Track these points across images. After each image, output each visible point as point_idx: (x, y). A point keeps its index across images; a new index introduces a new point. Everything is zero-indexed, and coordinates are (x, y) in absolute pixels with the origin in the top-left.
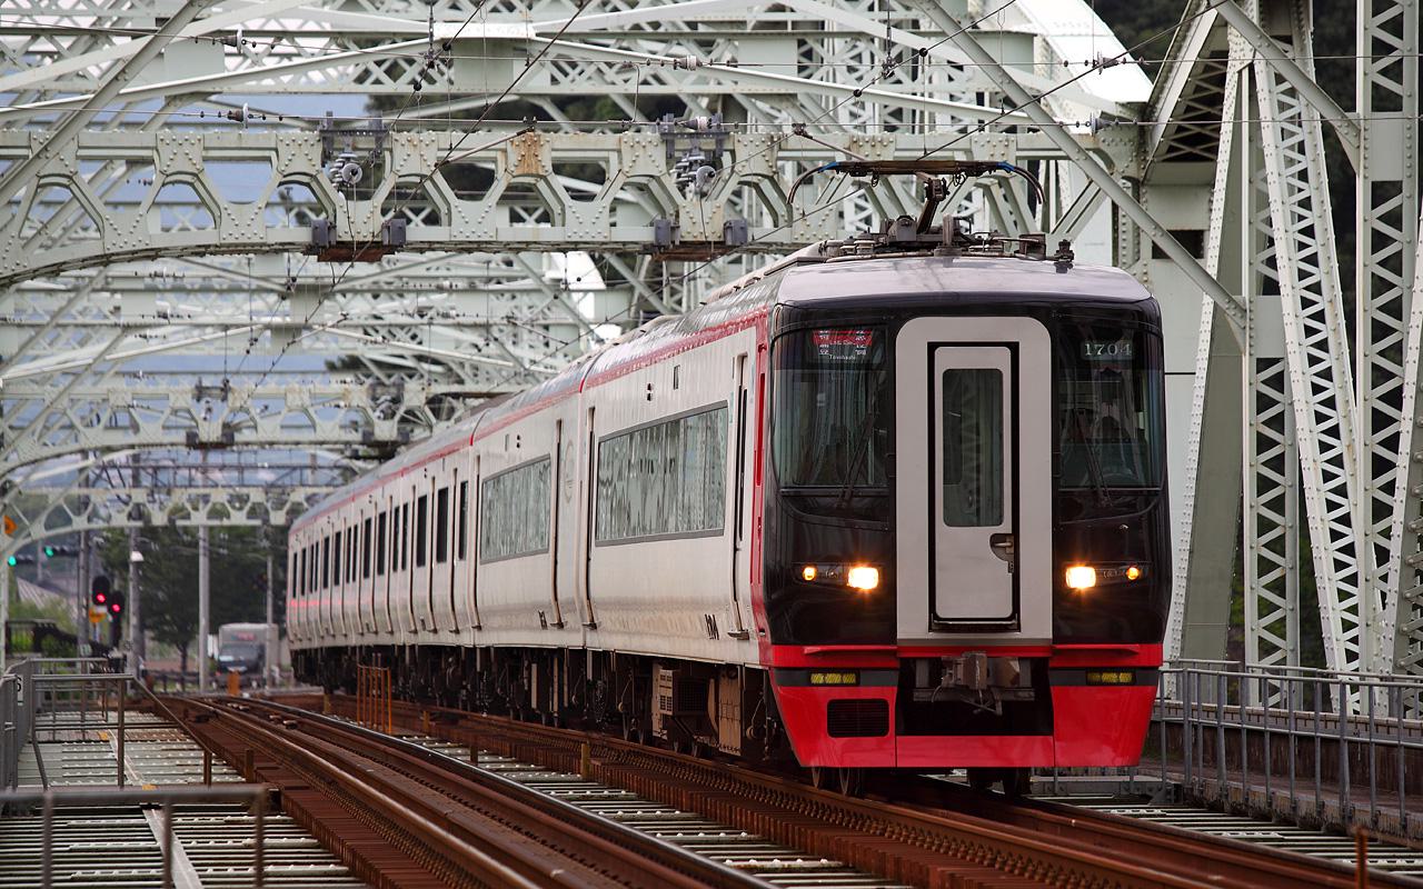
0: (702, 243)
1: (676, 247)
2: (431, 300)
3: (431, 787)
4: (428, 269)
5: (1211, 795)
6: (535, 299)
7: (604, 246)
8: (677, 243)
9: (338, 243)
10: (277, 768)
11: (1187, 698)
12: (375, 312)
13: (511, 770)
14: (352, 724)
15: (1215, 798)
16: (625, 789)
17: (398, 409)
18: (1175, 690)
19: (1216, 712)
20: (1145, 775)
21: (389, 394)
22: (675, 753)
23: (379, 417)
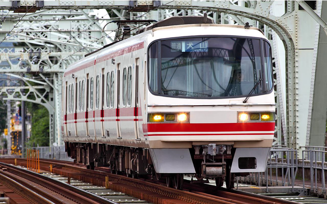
0: (145, 6)
1: (137, 7)
2: (50, 23)
3: (55, 192)
4: (49, 12)
5: (320, 192)
6: (86, 22)
7: (112, 7)
8: (137, 6)
9: (21, 6)
10: (2, 185)
11: (312, 159)
12: (31, 28)
13: (81, 185)
14: (25, 169)
15: (321, 194)
16: (121, 192)
17: (39, 60)
18: (307, 157)
19: (321, 164)
20: (297, 186)
21: (36, 55)
22: (127, 177)
23: (33, 63)
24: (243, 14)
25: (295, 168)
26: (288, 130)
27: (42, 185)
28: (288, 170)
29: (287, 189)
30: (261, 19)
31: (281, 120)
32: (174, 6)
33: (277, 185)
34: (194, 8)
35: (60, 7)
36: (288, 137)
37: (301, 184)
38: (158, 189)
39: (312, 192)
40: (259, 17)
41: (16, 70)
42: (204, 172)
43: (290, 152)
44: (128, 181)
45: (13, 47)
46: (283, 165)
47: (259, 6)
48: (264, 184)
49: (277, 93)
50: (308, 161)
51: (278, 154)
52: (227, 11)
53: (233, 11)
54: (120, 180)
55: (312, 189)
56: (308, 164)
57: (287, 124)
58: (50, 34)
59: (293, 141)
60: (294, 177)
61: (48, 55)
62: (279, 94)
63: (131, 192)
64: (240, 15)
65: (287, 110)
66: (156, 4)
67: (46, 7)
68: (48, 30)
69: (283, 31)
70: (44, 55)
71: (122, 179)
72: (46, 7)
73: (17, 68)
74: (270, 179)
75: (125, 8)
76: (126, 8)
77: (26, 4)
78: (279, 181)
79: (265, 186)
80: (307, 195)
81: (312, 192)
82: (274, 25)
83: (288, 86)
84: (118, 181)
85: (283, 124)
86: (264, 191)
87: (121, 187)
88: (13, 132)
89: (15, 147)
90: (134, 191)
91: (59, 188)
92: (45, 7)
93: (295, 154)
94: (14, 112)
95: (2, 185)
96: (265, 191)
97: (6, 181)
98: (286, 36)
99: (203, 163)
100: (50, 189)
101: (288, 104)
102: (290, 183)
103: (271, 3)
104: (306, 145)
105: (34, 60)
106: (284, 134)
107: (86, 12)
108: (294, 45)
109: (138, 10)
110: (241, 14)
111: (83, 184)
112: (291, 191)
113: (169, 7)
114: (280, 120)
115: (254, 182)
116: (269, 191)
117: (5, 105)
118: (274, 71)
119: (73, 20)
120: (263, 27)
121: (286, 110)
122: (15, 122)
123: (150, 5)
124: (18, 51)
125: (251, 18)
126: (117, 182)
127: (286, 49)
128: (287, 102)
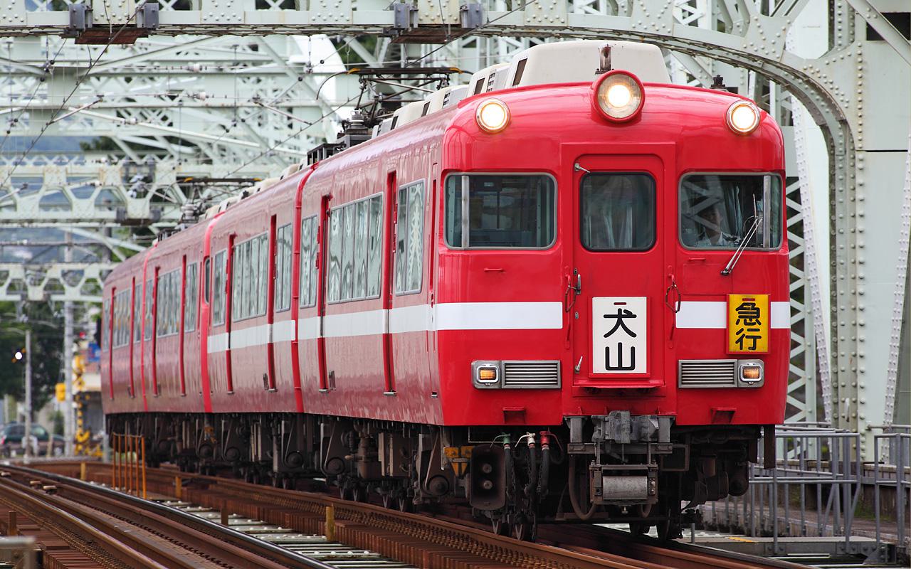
0: (439, 26)
3: (185, 547)
7: (347, 29)
9: (94, 25)
10: (39, 530)
13: (260, 533)
16: (368, 549)
20: (859, 535)
21: (142, 174)
23: (132, 196)
24: (710, 52)
25: (854, 486)
26: (834, 379)
27: (149, 530)
28: (835, 490)
29: (832, 544)
30: (760, 66)
31: (817, 351)
32: (519, 27)
33: (804, 534)
34: (576, 32)
35: (203, 29)
36: (835, 400)
37: (870, 530)
38: (472, 542)
39: (902, 552)
40: (755, 61)
41: (87, 214)
42: (598, 491)
43: (841, 439)
44: (390, 519)
45: (80, 153)
46: (823, 476)
47: (759, 34)
48: (768, 531)
49: (804, 309)
50: (891, 466)
51: (807, 448)
52: (666, 42)
53: (684, 42)
54: (367, 517)
55: (901, 544)
56: (891, 474)
57: (832, 363)
58: (180, 113)
59: (848, 412)
60: (851, 509)
61: (175, 172)
62: (810, 277)
63: (396, 548)
64: (704, 54)
65: (834, 323)
66: (470, 21)
67: (164, 27)
68: (176, 102)
69: (823, 101)
70: (163, 174)
71: (372, 513)
72: (164, 27)
73: (88, 207)
74: (784, 518)
75: (382, 32)
76: (388, 32)
77: (108, 20)
78: (811, 523)
79: (771, 535)
80: (886, 561)
81: (902, 552)
82: (797, 83)
83: (835, 255)
84: (362, 519)
85: (821, 363)
86: (766, 549)
87: (368, 535)
88: (80, 393)
89: (86, 436)
90: (404, 546)
91: (194, 537)
92: (161, 27)
93: (855, 448)
94: (83, 337)
95: (39, 530)
96: (770, 550)
97: (51, 517)
98: (831, 114)
99: (592, 464)
100: (171, 540)
101: (836, 306)
102: (839, 528)
103: (788, 21)
104: (884, 422)
105: (135, 186)
106: (823, 390)
107: (280, 55)
108: (853, 138)
109: (421, 38)
110: (705, 50)
111: (265, 528)
112: (842, 550)
113: (505, 31)
114: (812, 352)
115: (739, 525)
116: (782, 550)
117: (59, 316)
118: (798, 215)
119: (243, 76)
120: (766, 90)
121: (831, 322)
122: (86, 365)
123: (454, 23)
124: (93, 165)
125: (735, 64)
126: (360, 522)
127: (832, 152)
128: (834, 301)
